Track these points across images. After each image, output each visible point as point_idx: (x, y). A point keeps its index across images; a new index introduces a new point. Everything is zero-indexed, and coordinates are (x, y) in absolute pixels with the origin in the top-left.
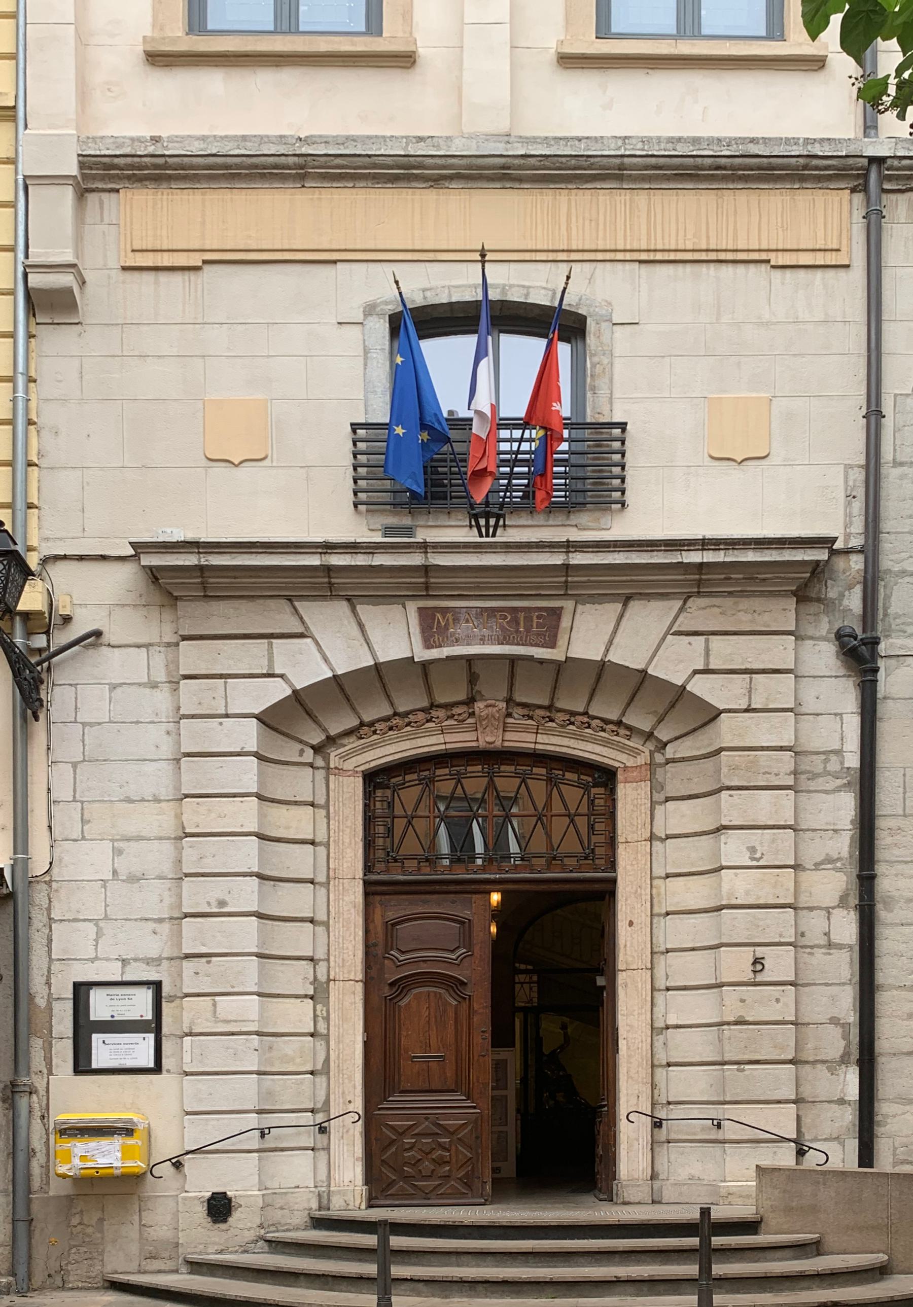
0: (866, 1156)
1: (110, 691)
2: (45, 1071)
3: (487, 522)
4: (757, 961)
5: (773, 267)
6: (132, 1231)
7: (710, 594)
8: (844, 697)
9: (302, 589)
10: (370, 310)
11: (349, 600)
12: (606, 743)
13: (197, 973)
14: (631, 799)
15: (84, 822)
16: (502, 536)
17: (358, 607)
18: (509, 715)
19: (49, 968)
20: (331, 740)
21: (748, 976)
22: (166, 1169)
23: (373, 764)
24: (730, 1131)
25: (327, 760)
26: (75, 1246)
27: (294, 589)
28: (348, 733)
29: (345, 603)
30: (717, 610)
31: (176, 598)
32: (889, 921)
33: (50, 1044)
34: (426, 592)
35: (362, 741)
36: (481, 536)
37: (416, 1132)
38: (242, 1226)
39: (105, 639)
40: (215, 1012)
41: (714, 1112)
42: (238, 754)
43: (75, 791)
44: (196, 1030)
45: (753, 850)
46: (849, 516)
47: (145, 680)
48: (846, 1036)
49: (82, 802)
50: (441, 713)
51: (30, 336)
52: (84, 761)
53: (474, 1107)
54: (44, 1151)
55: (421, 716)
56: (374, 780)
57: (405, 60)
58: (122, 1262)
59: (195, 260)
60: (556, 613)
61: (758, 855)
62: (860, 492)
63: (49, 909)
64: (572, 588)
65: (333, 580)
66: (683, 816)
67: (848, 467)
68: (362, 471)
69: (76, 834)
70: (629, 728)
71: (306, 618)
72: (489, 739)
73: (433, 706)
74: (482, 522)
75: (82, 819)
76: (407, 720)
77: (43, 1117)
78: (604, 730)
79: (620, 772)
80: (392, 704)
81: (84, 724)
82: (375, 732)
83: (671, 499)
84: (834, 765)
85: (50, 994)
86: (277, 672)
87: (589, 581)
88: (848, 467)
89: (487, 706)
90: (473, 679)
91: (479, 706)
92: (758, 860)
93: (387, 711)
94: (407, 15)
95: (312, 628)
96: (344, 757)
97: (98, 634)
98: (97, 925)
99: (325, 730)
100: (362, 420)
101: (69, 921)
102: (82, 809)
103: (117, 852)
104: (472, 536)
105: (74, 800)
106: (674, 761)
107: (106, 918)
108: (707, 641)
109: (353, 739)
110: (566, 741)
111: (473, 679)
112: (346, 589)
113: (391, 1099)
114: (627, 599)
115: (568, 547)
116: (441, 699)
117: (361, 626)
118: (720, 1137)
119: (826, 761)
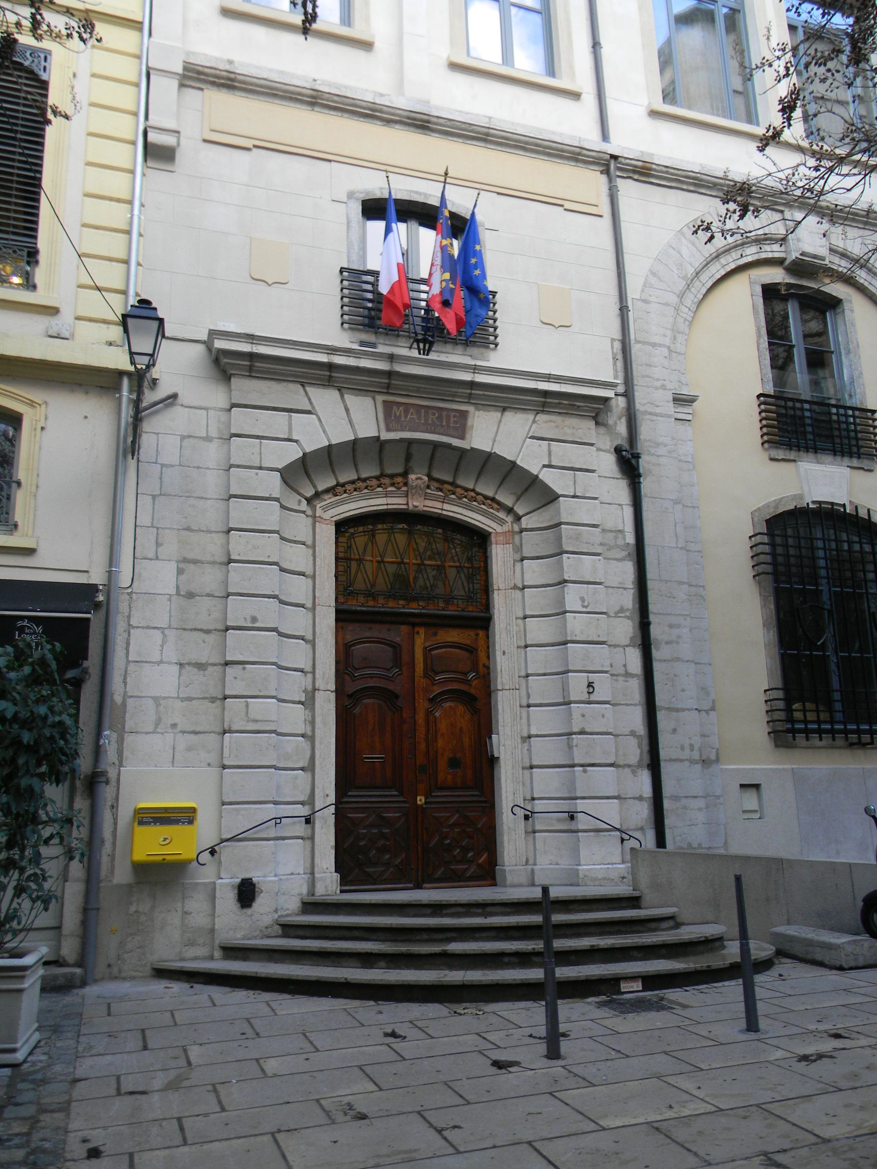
0: (661, 842)
1: (182, 440)
2: (117, 763)
3: (424, 347)
4: (590, 685)
5: (566, 210)
6: (175, 919)
7: (549, 412)
8: (620, 491)
9: (312, 378)
10: (351, 195)
11: (339, 390)
12: (485, 514)
13: (235, 678)
14: (500, 557)
15: (158, 544)
16: (433, 356)
17: (346, 396)
18: (428, 487)
19: (126, 668)
20: (317, 495)
21: (585, 697)
22: (205, 857)
23: (342, 516)
24: (583, 821)
25: (314, 510)
26: (131, 934)
27: (306, 378)
28: (327, 491)
29: (337, 392)
30: (553, 424)
31: (231, 375)
32: (658, 658)
33: (123, 736)
34: (388, 389)
35: (338, 498)
36: (420, 354)
37: (367, 823)
38: (262, 912)
39: (180, 400)
40: (247, 713)
41: (565, 805)
42: (267, 499)
43: (153, 519)
44: (234, 728)
45: (583, 600)
46: (616, 371)
47: (205, 435)
48: (640, 746)
49: (158, 528)
50: (387, 481)
51: (144, 175)
52: (161, 494)
53: (405, 802)
54: (111, 840)
55: (374, 482)
56: (342, 526)
57: (366, 45)
58: (167, 948)
59: (248, 143)
60: (464, 415)
61: (586, 604)
62: (620, 356)
63: (129, 617)
64: (475, 399)
65: (333, 374)
66: (534, 572)
67: (613, 340)
68: (346, 300)
69: (151, 555)
70: (499, 503)
71: (313, 400)
72: (415, 504)
73: (383, 475)
74: (421, 345)
75: (157, 543)
76: (365, 484)
77: (113, 807)
78: (484, 504)
79: (493, 536)
80: (357, 471)
81: (162, 465)
82: (345, 492)
83: (522, 348)
84: (620, 542)
85: (125, 692)
86: (295, 438)
87: (484, 395)
88: (613, 340)
89: (417, 479)
90: (408, 458)
91: (412, 477)
92: (586, 607)
93: (354, 477)
94: (367, 20)
95: (317, 408)
96: (325, 509)
97: (174, 396)
98: (163, 633)
99: (315, 487)
100: (346, 266)
101: (143, 628)
102: (158, 534)
103: (180, 572)
104: (414, 353)
105: (152, 526)
106: (527, 530)
107: (170, 627)
108: (549, 445)
109: (330, 495)
110: (460, 510)
111: (408, 458)
112: (339, 382)
113: (350, 793)
114: (504, 409)
115: (475, 369)
116: (389, 471)
117: (347, 410)
118: (573, 828)
119: (616, 538)
